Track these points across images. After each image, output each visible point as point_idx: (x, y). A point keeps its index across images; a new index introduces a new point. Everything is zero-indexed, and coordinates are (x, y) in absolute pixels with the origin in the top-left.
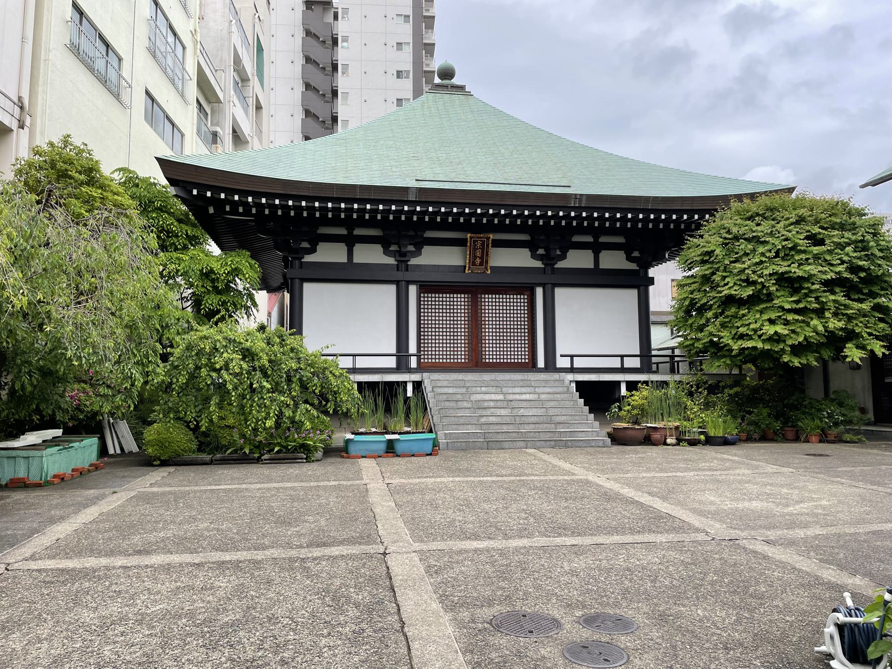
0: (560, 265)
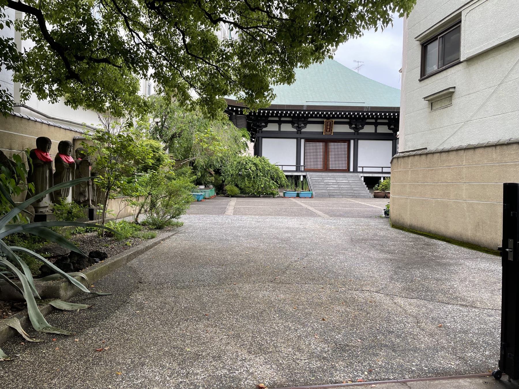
0: (361, 131)
